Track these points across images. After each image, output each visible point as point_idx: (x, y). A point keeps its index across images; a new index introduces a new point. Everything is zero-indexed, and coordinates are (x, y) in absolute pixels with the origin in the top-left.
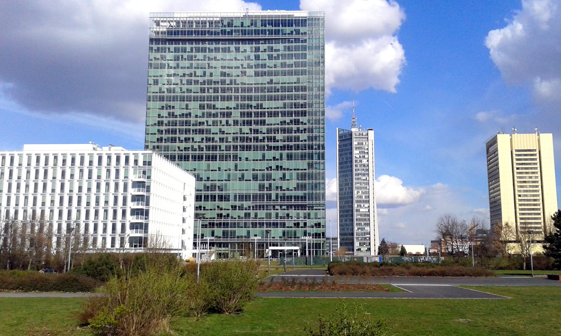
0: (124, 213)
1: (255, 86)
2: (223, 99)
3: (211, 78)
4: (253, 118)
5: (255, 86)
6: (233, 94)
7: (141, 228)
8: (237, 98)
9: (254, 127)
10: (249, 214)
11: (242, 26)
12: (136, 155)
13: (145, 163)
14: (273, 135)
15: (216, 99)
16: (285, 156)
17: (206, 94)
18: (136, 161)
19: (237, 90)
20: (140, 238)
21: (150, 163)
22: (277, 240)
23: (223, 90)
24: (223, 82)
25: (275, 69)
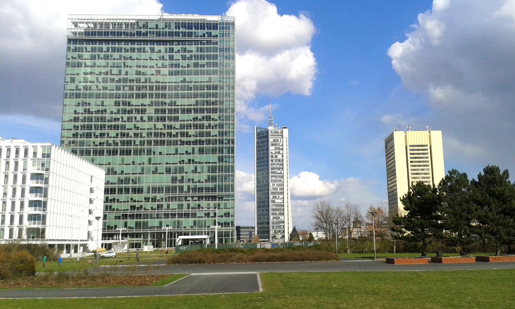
2: (138, 96)
3: (126, 76)
6: (148, 92)
8: (151, 96)
9: (167, 123)
12: (35, 147)
13: (43, 155)
15: (131, 96)
18: (35, 154)
21: (49, 156)
22: (189, 229)
24: (138, 81)
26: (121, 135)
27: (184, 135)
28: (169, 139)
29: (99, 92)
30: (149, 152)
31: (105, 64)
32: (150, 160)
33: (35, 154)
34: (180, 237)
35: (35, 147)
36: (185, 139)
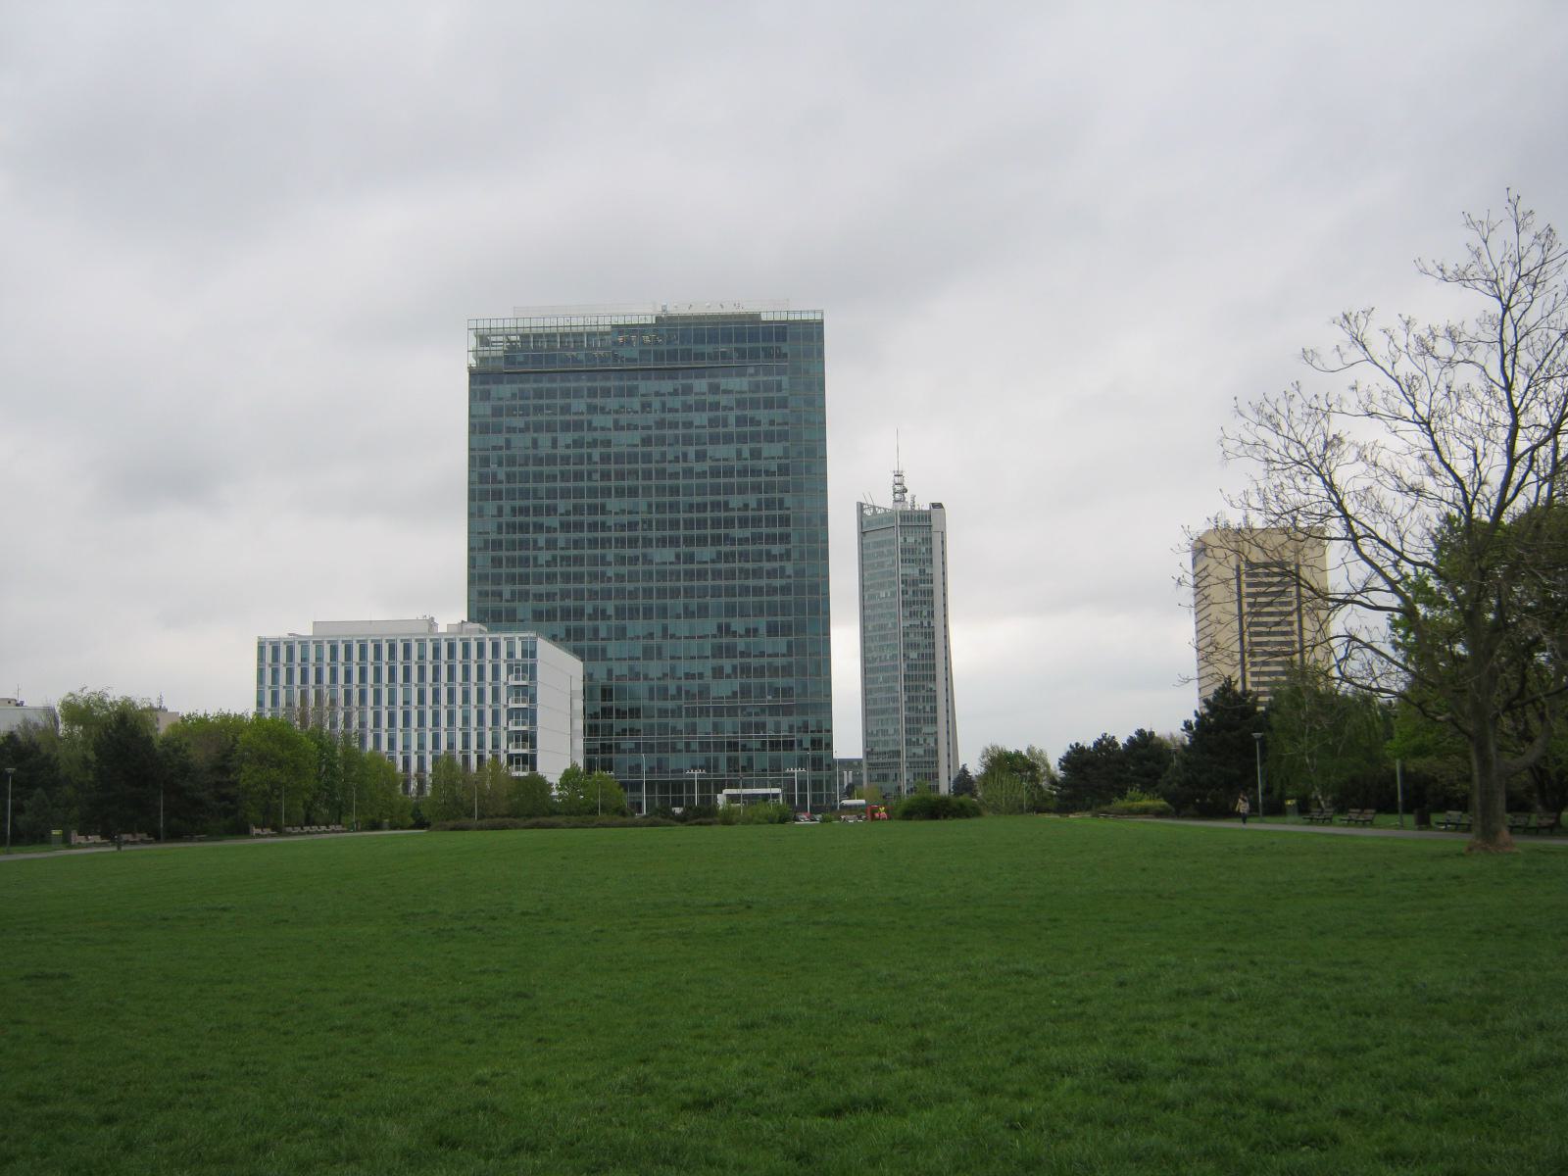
0: (496, 715)
1: (481, 453)
2: (620, 492)
3: (554, 451)
4: (682, 532)
5: (481, 453)
6: (641, 482)
7: (525, 762)
8: (647, 490)
9: (683, 549)
10: (556, 541)
11: (508, 447)
12: (510, 643)
13: (524, 653)
14: (599, 501)
15: (606, 492)
16: (763, 630)
17: (585, 484)
18: (511, 654)
19: (647, 475)
20: (525, 756)
21: (533, 654)
22: (723, 776)
23: (620, 475)
24: (647, 458)
25: (508, 452)
26: (562, 596)
27: (596, 577)
28: (661, 584)
29: (499, 486)
30: (663, 612)
31: (522, 426)
32: (665, 629)
33: (511, 654)
34: (726, 791)
35: (510, 643)
36: (598, 586)
